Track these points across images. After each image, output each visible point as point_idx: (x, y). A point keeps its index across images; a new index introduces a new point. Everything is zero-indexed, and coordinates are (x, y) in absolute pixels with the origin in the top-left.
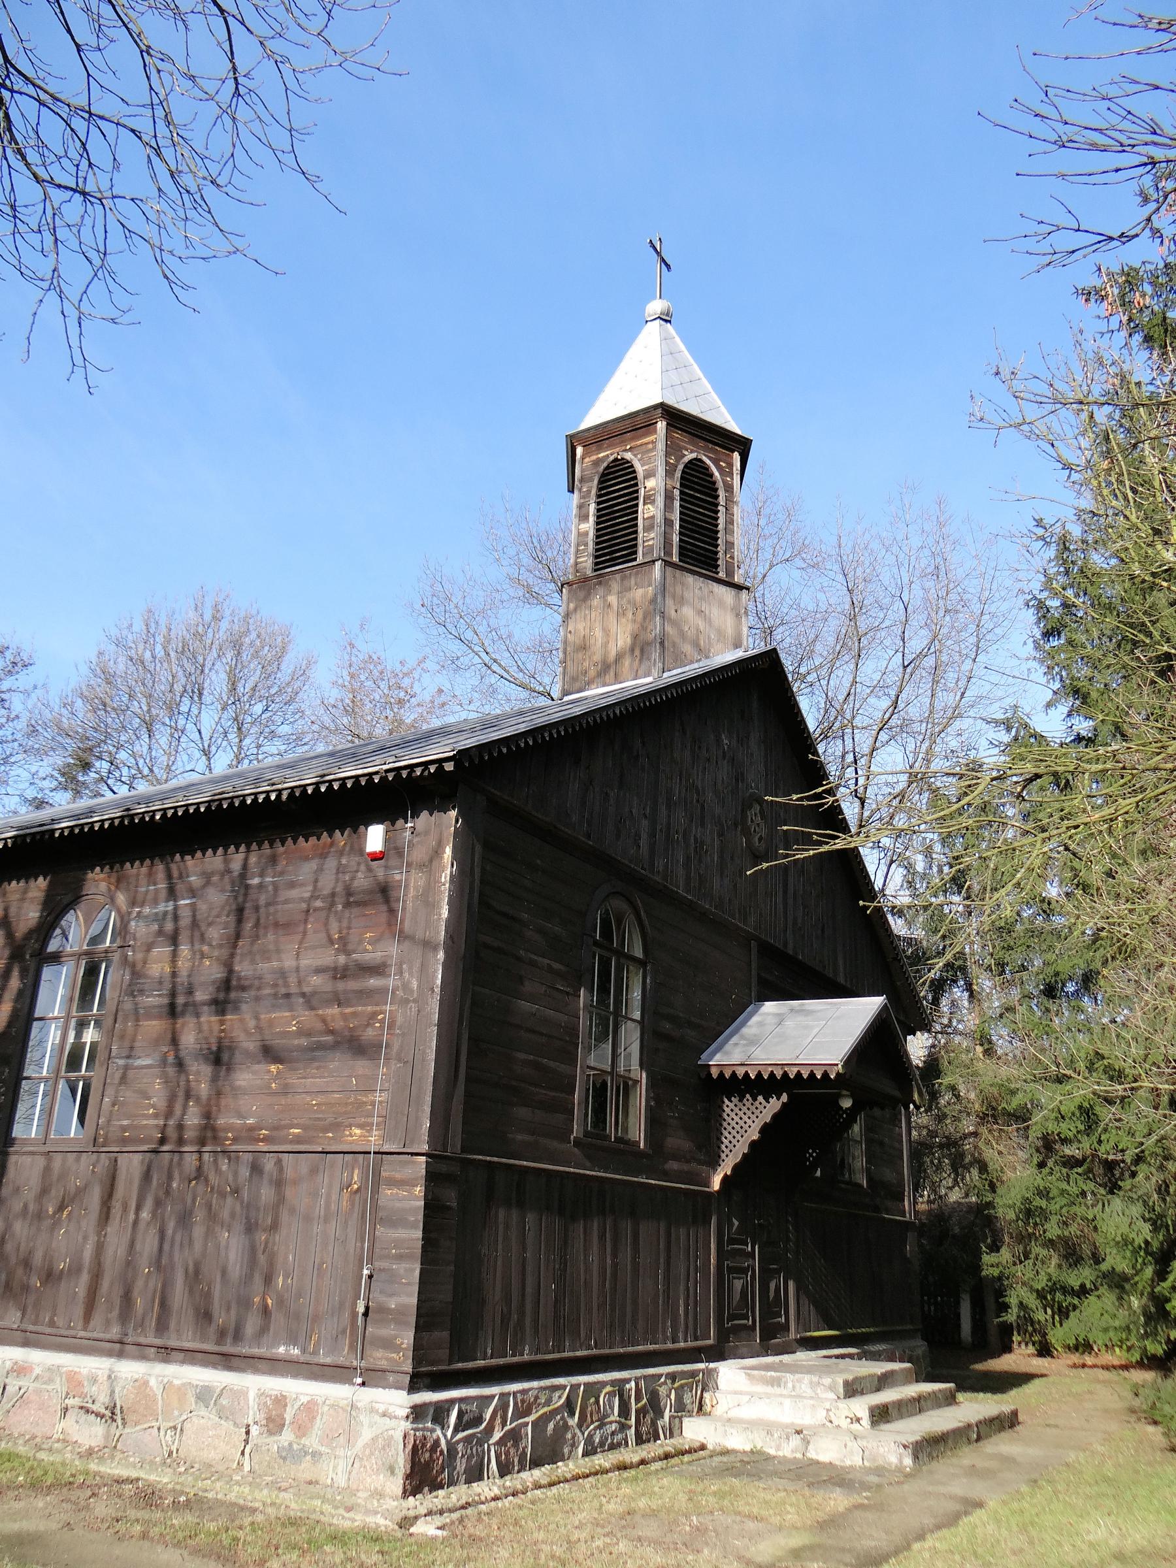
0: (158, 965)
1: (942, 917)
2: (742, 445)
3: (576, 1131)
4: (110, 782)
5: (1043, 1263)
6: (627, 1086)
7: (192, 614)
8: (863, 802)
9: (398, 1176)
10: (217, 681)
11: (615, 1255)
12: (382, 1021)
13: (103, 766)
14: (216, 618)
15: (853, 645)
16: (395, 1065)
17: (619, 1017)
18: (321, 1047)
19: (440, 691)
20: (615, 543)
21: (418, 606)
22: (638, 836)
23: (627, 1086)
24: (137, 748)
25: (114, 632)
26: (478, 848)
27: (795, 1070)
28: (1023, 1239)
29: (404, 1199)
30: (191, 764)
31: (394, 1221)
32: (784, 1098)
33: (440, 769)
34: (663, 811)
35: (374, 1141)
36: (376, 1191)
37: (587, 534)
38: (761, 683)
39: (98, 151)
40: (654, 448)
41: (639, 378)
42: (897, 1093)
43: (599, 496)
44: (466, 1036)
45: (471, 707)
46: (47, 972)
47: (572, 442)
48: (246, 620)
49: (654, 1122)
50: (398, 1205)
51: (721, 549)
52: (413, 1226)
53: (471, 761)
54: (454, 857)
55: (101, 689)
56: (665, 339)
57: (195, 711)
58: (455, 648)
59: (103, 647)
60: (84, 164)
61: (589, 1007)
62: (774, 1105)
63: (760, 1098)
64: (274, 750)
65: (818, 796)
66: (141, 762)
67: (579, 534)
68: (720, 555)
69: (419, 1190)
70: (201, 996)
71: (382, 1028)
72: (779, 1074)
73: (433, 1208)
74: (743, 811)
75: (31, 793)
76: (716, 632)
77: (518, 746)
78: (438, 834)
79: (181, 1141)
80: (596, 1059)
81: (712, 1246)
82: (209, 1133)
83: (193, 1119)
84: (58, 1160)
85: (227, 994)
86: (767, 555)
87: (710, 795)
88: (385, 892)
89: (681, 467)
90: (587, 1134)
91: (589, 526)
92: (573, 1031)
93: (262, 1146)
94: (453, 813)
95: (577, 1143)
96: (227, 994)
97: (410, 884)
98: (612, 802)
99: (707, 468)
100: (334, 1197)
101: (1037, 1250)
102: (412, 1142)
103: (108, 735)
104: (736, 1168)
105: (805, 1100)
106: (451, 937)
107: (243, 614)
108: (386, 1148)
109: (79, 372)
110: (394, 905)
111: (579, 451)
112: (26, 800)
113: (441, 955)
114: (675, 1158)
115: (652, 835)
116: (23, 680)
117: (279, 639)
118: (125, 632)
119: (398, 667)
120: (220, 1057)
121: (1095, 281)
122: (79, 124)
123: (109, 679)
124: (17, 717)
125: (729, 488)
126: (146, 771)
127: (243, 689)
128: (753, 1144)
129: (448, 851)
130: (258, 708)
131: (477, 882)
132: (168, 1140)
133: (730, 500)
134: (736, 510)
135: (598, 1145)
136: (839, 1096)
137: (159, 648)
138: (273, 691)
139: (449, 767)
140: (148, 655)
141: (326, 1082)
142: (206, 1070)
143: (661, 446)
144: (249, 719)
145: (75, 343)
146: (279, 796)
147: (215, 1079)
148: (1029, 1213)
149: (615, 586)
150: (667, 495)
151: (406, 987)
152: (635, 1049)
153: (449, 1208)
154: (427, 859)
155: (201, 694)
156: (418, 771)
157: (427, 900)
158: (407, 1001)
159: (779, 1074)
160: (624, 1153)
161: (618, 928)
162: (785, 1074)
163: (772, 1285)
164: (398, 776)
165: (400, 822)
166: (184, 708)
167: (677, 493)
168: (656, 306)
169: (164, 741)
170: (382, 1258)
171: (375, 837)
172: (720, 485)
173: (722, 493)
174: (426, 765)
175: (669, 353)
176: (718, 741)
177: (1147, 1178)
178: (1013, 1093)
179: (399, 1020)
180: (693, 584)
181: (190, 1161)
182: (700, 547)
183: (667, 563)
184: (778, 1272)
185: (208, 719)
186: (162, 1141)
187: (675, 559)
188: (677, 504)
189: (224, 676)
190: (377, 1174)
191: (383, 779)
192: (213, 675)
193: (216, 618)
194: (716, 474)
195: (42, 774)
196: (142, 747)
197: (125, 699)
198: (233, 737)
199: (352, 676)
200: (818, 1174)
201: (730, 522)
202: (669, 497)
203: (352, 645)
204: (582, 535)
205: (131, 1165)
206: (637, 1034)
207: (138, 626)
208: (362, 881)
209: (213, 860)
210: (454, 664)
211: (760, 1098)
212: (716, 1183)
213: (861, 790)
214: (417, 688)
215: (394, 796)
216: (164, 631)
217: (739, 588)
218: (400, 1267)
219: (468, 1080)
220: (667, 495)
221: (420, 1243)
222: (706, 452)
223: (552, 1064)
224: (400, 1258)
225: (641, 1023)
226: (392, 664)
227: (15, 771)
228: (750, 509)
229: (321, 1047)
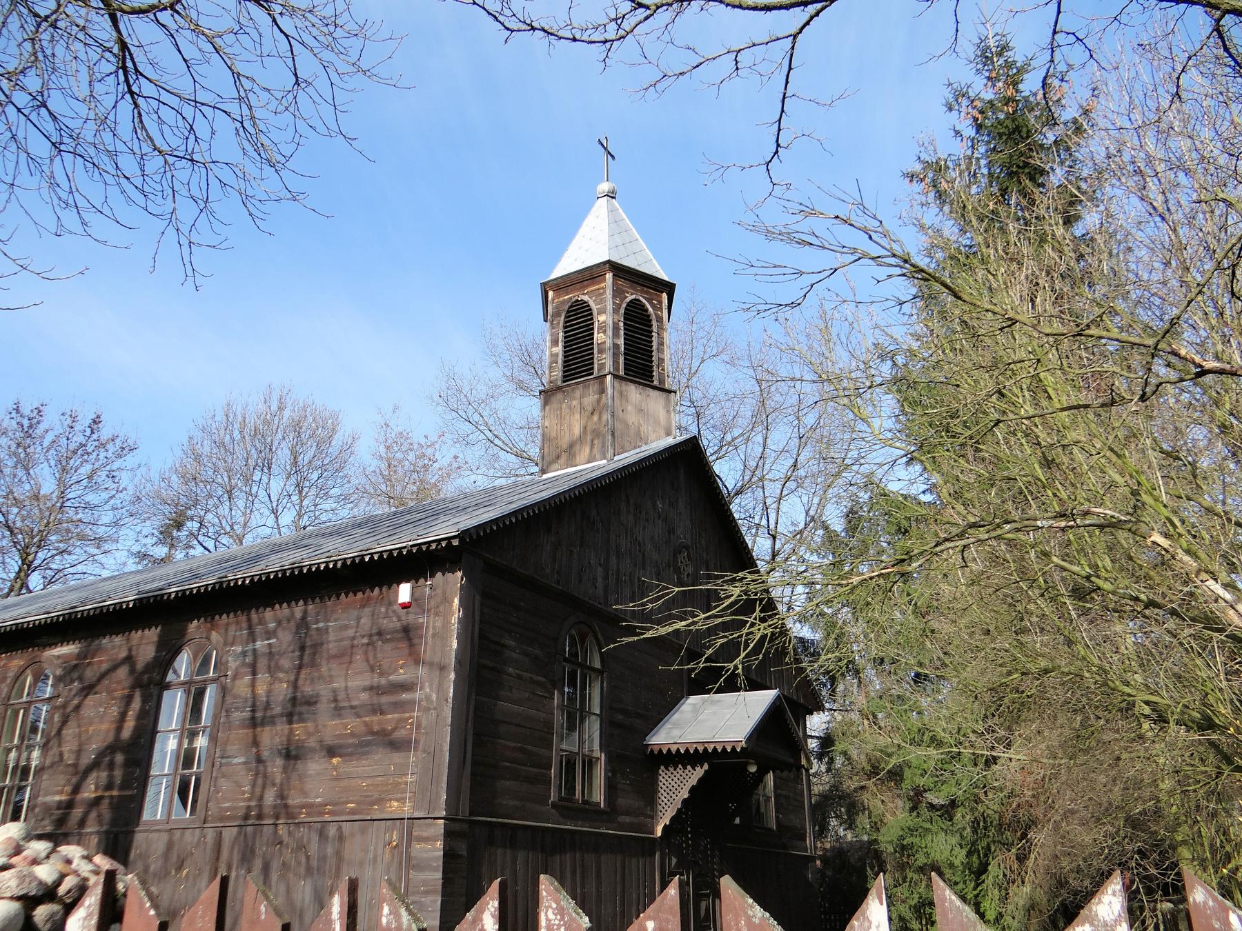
0: (242, 687)
1: (834, 624)
2: (669, 288)
3: (553, 796)
4: (200, 538)
5: (916, 884)
6: (590, 762)
7: (260, 406)
8: (774, 538)
9: (425, 834)
10: (283, 456)
11: (583, 886)
12: (412, 724)
13: (192, 525)
14: (281, 408)
15: (763, 418)
16: (421, 755)
17: (584, 713)
18: (368, 744)
19: (456, 457)
20: (577, 361)
21: (436, 397)
22: (595, 579)
23: (590, 762)
24: (220, 512)
25: (201, 422)
26: (478, 597)
27: (712, 746)
28: (902, 867)
29: (430, 850)
30: (264, 528)
31: (420, 867)
32: (706, 766)
33: (449, 544)
34: (614, 559)
35: (407, 810)
36: (409, 846)
37: (557, 355)
38: (688, 460)
39: (202, 128)
40: (604, 293)
41: (588, 246)
42: (792, 761)
43: (565, 327)
44: (471, 732)
45: (479, 471)
46: (166, 694)
47: (545, 288)
48: (304, 408)
49: (611, 787)
50: (425, 855)
51: (655, 363)
52: (436, 870)
53: (471, 537)
54: (461, 605)
55: (191, 469)
56: (612, 211)
57: (265, 479)
58: (467, 428)
59: (192, 433)
60: (192, 137)
61: (561, 707)
62: (699, 772)
63: (689, 767)
64: (327, 507)
65: (643, 605)
66: (224, 522)
67: (552, 355)
68: (655, 368)
69: (439, 844)
70: (278, 710)
71: (411, 729)
72: (701, 749)
73: (450, 856)
74: (675, 555)
75: (136, 548)
76: (652, 427)
77: (504, 524)
78: (450, 585)
79: (260, 816)
80: (569, 745)
81: (657, 878)
82: (284, 810)
83: (270, 798)
84: (178, 834)
85: (297, 707)
86: (698, 351)
87: (649, 547)
88: (408, 633)
89: (624, 306)
90: (561, 799)
91: (559, 349)
92: (549, 725)
93: (327, 818)
94: (459, 574)
95: (554, 806)
96: (297, 707)
97: (429, 624)
98: (575, 556)
99: (644, 306)
100: (380, 852)
101: (910, 875)
102: (434, 809)
103: (196, 502)
104: (672, 820)
105: (723, 769)
106: (459, 661)
107: (301, 405)
108: (416, 815)
109: (190, 280)
110: (416, 641)
111: (551, 294)
112: (133, 554)
113: (452, 676)
114: (627, 813)
115: (606, 578)
116: (130, 460)
117: (330, 422)
118: (210, 421)
119: (423, 441)
120: (292, 754)
121: (918, 167)
122: (188, 111)
123: (198, 458)
124: (125, 489)
125: (660, 319)
126: (228, 529)
127: (304, 460)
128: (684, 801)
129: (456, 601)
130: (315, 476)
131: (477, 622)
132: (251, 818)
133: (660, 328)
134: (665, 335)
135: (568, 808)
136: (747, 764)
137: (236, 433)
138: (326, 462)
139: (456, 543)
140: (227, 438)
141: (370, 769)
142: (279, 762)
143: (609, 292)
144: (307, 484)
145: (187, 260)
146: (335, 565)
147: (285, 770)
148: (903, 848)
149: (578, 393)
150: (613, 328)
151: (428, 698)
152: (597, 735)
153: (461, 856)
154: (441, 610)
155: (269, 468)
156: (434, 546)
157: (441, 636)
158: (429, 709)
159: (701, 749)
160: (588, 811)
161: (582, 647)
162: (706, 749)
163: (703, 904)
164: (420, 549)
165: (422, 581)
166: (256, 478)
167: (621, 324)
168: (605, 187)
169: (241, 504)
170: (414, 894)
171: (404, 592)
172: (653, 317)
173: (654, 323)
174: (439, 541)
175: (614, 221)
176: (655, 505)
177: (963, 816)
178: (890, 755)
179: (424, 723)
180: (634, 392)
181: (268, 831)
182: (640, 364)
183: (616, 377)
184: (707, 896)
185: (276, 486)
186: (246, 817)
187: (621, 373)
188: (622, 332)
189: (287, 452)
190: (410, 834)
191: (409, 552)
192: (279, 452)
193: (281, 408)
194: (650, 309)
195: (145, 532)
196: (224, 510)
197: (210, 473)
198: (295, 498)
199: (388, 448)
200: (737, 821)
201: (661, 344)
202: (616, 328)
203: (387, 425)
204: (554, 356)
205: (229, 834)
206: (596, 727)
207: (220, 416)
208: (394, 624)
209: (283, 611)
210: (464, 440)
211: (689, 767)
212: (659, 832)
213: (772, 526)
214: (438, 456)
215: (417, 563)
216: (240, 419)
217: (669, 392)
218: (427, 900)
219: (474, 763)
220: (613, 328)
221: (441, 882)
222: (642, 297)
223: (534, 749)
224: (427, 893)
225: (600, 716)
226: (417, 437)
227: (124, 531)
228: (675, 338)
229: (368, 744)
